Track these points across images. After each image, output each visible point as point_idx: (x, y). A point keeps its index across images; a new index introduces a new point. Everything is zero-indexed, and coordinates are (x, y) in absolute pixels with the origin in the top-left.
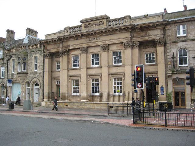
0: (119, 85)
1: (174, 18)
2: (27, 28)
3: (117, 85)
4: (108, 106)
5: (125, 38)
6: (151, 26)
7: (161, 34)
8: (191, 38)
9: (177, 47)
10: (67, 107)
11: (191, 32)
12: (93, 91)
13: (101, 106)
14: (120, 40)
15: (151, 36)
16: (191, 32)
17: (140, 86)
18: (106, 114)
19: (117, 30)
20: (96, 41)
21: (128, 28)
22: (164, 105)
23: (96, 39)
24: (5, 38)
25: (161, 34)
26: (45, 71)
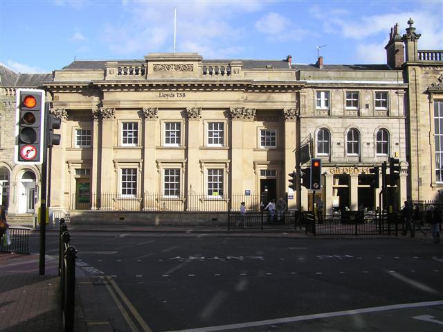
0: (175, 182)
1: (314, 78)
2: (386, 48)
3: (132, 181)
4: (229, 216)
5: (233, 101)
6: (134, 85)
7: (293, 102)
8: (336, 114)
9: (317, 125)
10: (123, 221)
11: (337, 105)
12: (165, 191)
13: (196, 218)
14: (224, 102)
15: (277, 102)
16: (337, 105)
17: (317, 186)
18: (227, 230)
19: (221, 85)
20: (179, 98)
21: (242, 85)
22: (363, 217)
23: (176, 95)
24: (386, 63)
25: (293, 102)
26: (103, 146)
